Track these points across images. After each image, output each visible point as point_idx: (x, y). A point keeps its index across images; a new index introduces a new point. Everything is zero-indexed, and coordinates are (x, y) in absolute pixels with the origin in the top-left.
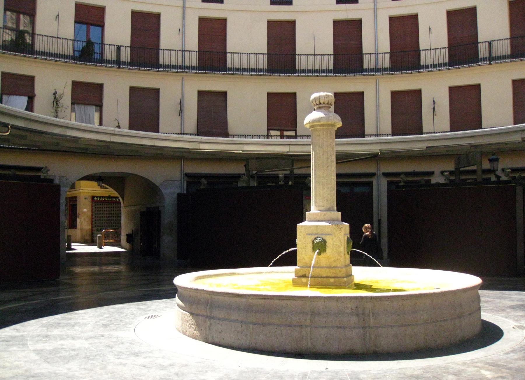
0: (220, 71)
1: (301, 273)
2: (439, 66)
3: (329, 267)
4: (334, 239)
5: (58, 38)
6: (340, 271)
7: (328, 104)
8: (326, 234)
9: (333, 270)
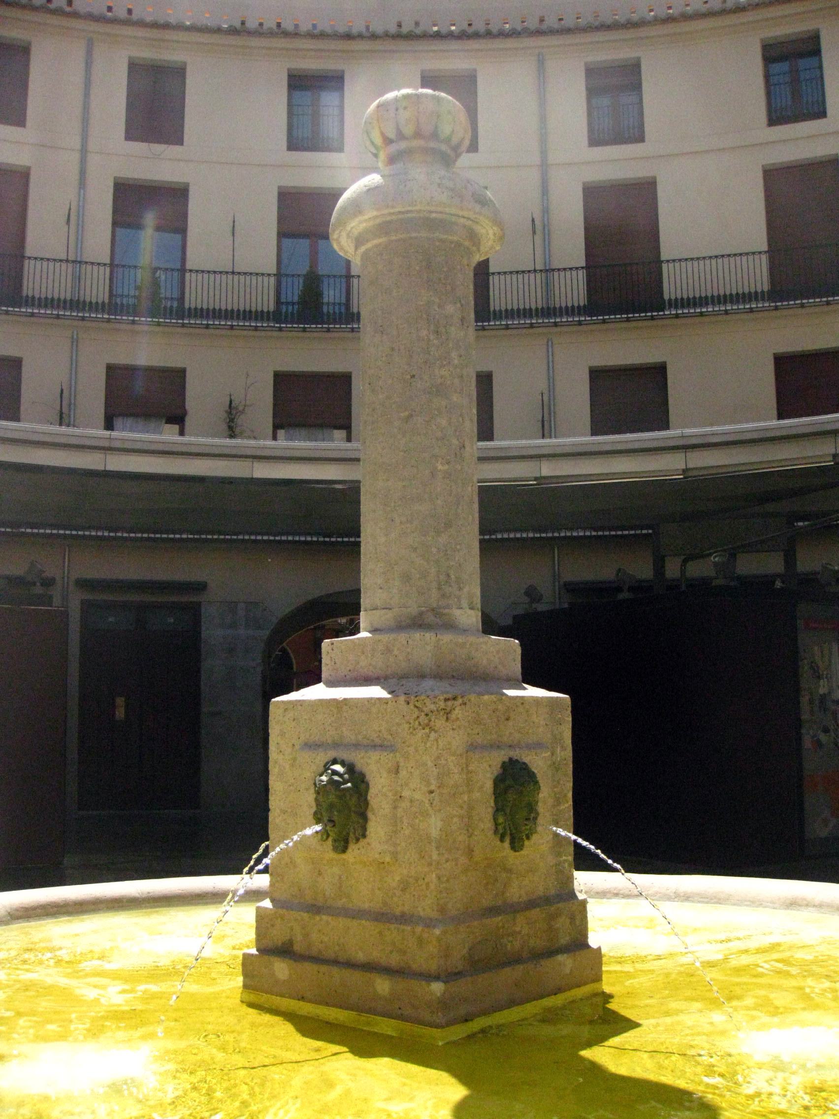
0: (640, 312)
1: (278, 936)
2: (537, 315)
3: (382, 917)
4: (403, 773)
5: (233, 273)
6: (420, 942)
7: (418, 135)
8: (529, 747)
9: (392, 933)
